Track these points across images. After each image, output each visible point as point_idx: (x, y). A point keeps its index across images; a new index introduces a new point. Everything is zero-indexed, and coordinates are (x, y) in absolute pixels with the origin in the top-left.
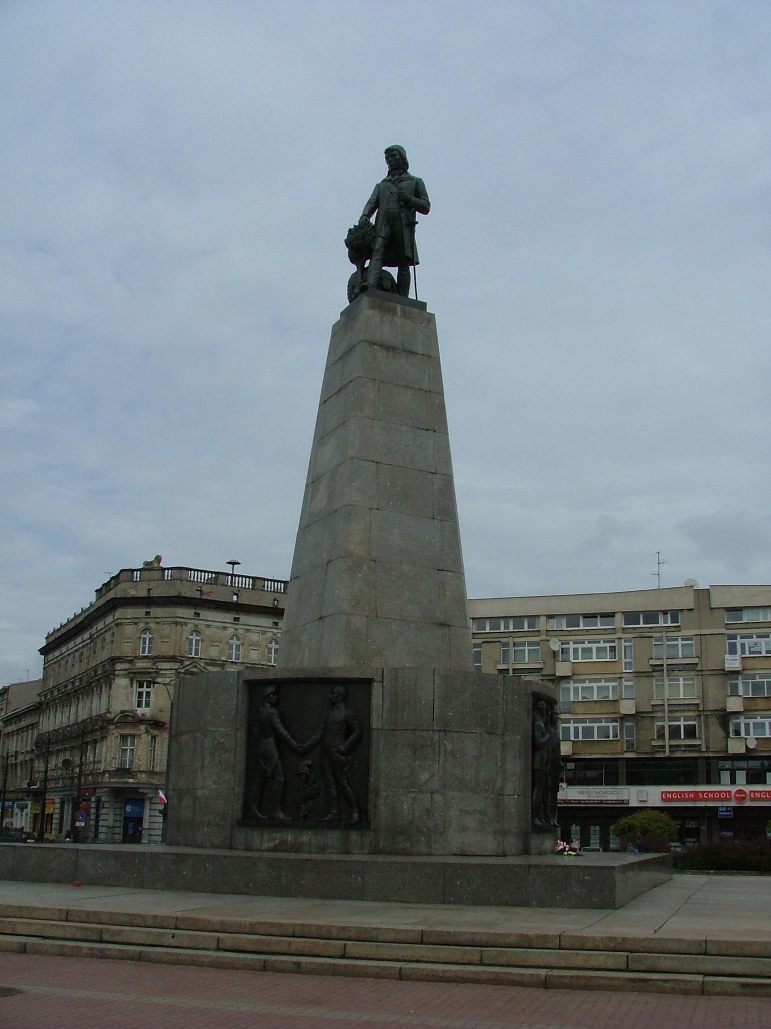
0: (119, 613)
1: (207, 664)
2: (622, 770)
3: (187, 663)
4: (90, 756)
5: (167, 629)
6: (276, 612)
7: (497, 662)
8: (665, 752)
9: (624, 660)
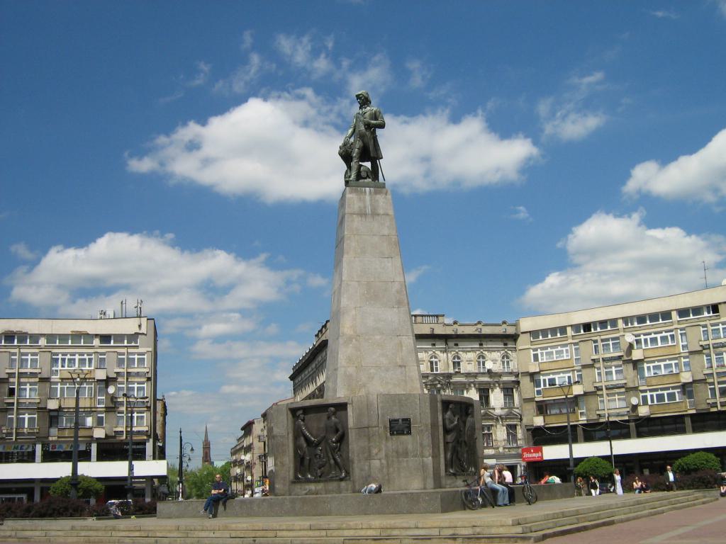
2: (580, 432)
8: (717, 407)
9: (681, 344)
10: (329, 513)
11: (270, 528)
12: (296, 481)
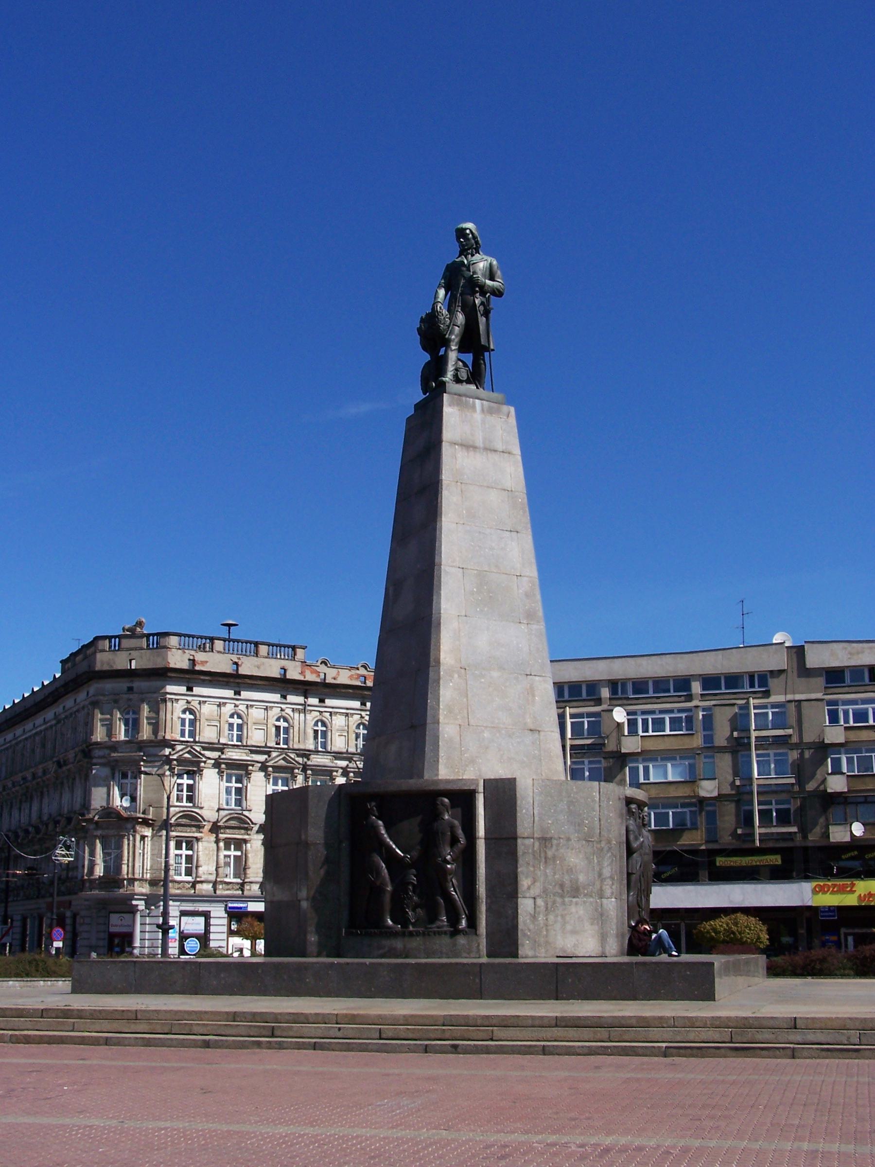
0: (94, 687)
1: (204, 749)
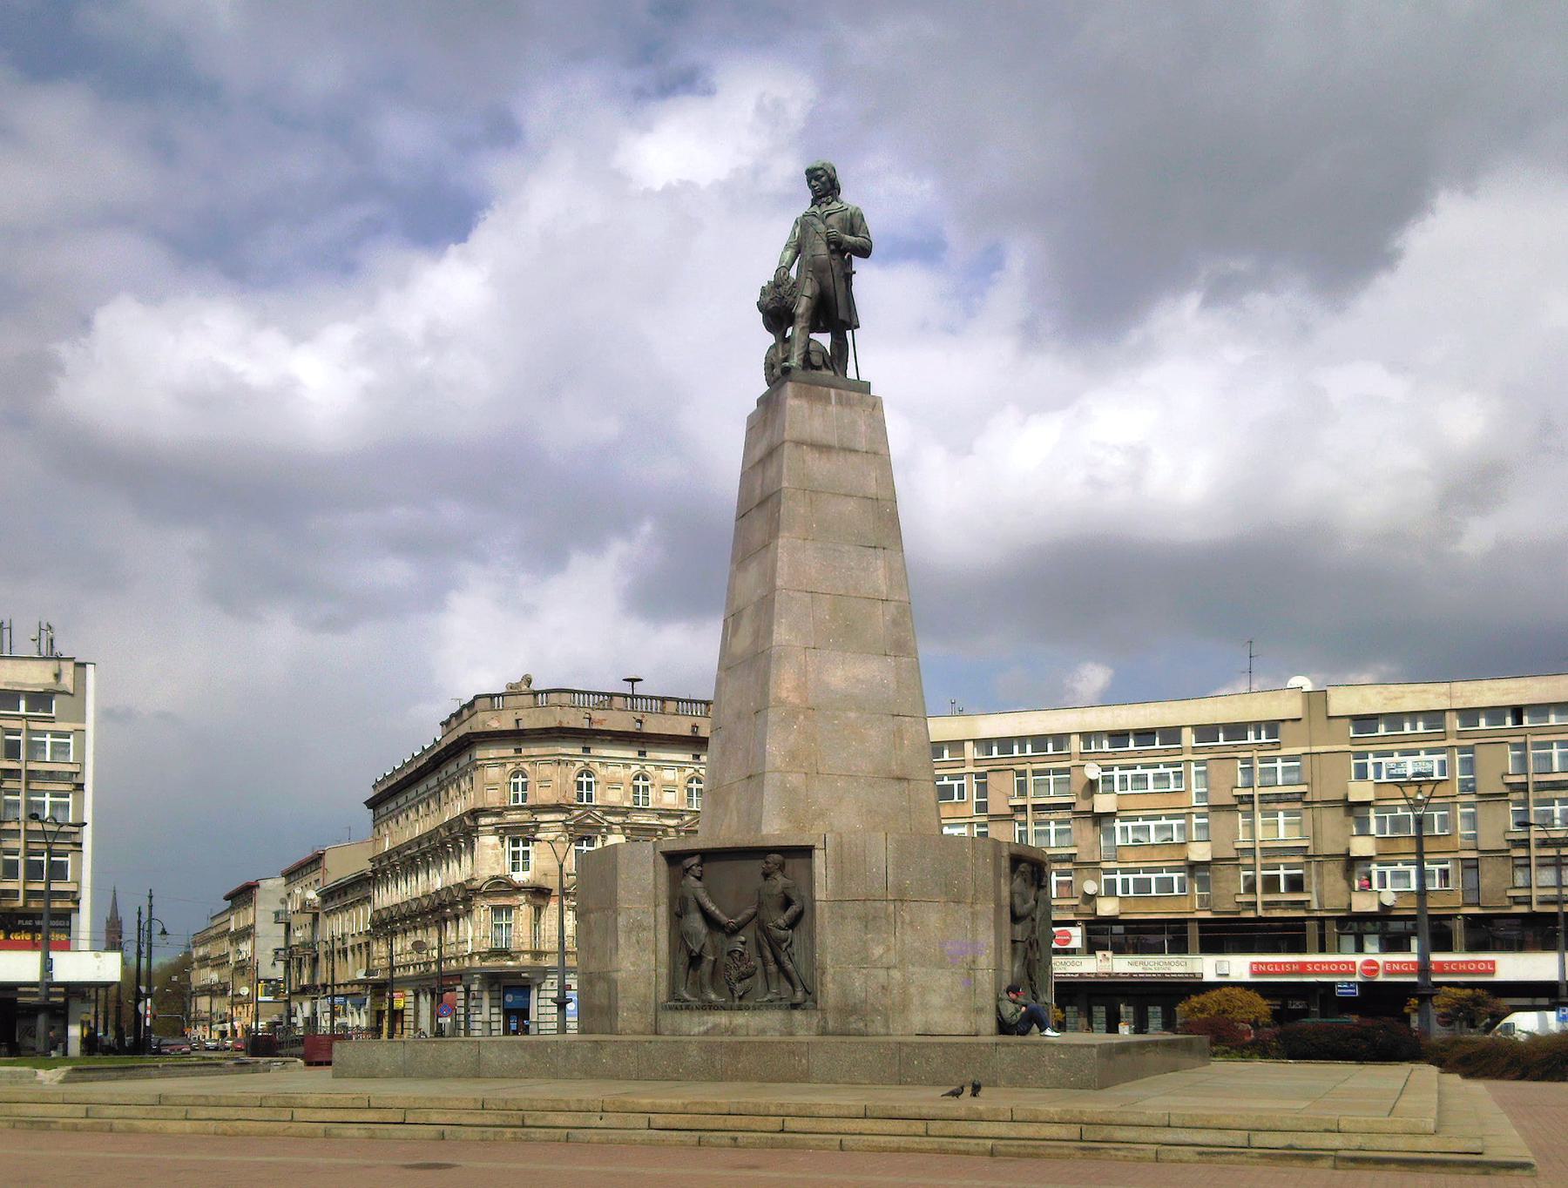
1: (605, 813)
2: (1194, 934)
3: (577, 813)
4: (450, 935)
5: (547, 770)
6: (695, 743)
7: (1012, 797)
9: (1194, 790)
10: (805, 1077)
11: (1268, 1125)
12: (676, 1003)
